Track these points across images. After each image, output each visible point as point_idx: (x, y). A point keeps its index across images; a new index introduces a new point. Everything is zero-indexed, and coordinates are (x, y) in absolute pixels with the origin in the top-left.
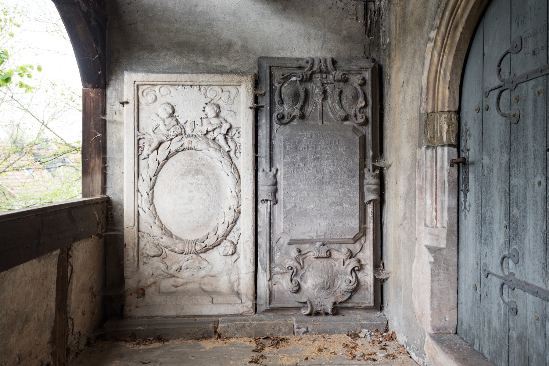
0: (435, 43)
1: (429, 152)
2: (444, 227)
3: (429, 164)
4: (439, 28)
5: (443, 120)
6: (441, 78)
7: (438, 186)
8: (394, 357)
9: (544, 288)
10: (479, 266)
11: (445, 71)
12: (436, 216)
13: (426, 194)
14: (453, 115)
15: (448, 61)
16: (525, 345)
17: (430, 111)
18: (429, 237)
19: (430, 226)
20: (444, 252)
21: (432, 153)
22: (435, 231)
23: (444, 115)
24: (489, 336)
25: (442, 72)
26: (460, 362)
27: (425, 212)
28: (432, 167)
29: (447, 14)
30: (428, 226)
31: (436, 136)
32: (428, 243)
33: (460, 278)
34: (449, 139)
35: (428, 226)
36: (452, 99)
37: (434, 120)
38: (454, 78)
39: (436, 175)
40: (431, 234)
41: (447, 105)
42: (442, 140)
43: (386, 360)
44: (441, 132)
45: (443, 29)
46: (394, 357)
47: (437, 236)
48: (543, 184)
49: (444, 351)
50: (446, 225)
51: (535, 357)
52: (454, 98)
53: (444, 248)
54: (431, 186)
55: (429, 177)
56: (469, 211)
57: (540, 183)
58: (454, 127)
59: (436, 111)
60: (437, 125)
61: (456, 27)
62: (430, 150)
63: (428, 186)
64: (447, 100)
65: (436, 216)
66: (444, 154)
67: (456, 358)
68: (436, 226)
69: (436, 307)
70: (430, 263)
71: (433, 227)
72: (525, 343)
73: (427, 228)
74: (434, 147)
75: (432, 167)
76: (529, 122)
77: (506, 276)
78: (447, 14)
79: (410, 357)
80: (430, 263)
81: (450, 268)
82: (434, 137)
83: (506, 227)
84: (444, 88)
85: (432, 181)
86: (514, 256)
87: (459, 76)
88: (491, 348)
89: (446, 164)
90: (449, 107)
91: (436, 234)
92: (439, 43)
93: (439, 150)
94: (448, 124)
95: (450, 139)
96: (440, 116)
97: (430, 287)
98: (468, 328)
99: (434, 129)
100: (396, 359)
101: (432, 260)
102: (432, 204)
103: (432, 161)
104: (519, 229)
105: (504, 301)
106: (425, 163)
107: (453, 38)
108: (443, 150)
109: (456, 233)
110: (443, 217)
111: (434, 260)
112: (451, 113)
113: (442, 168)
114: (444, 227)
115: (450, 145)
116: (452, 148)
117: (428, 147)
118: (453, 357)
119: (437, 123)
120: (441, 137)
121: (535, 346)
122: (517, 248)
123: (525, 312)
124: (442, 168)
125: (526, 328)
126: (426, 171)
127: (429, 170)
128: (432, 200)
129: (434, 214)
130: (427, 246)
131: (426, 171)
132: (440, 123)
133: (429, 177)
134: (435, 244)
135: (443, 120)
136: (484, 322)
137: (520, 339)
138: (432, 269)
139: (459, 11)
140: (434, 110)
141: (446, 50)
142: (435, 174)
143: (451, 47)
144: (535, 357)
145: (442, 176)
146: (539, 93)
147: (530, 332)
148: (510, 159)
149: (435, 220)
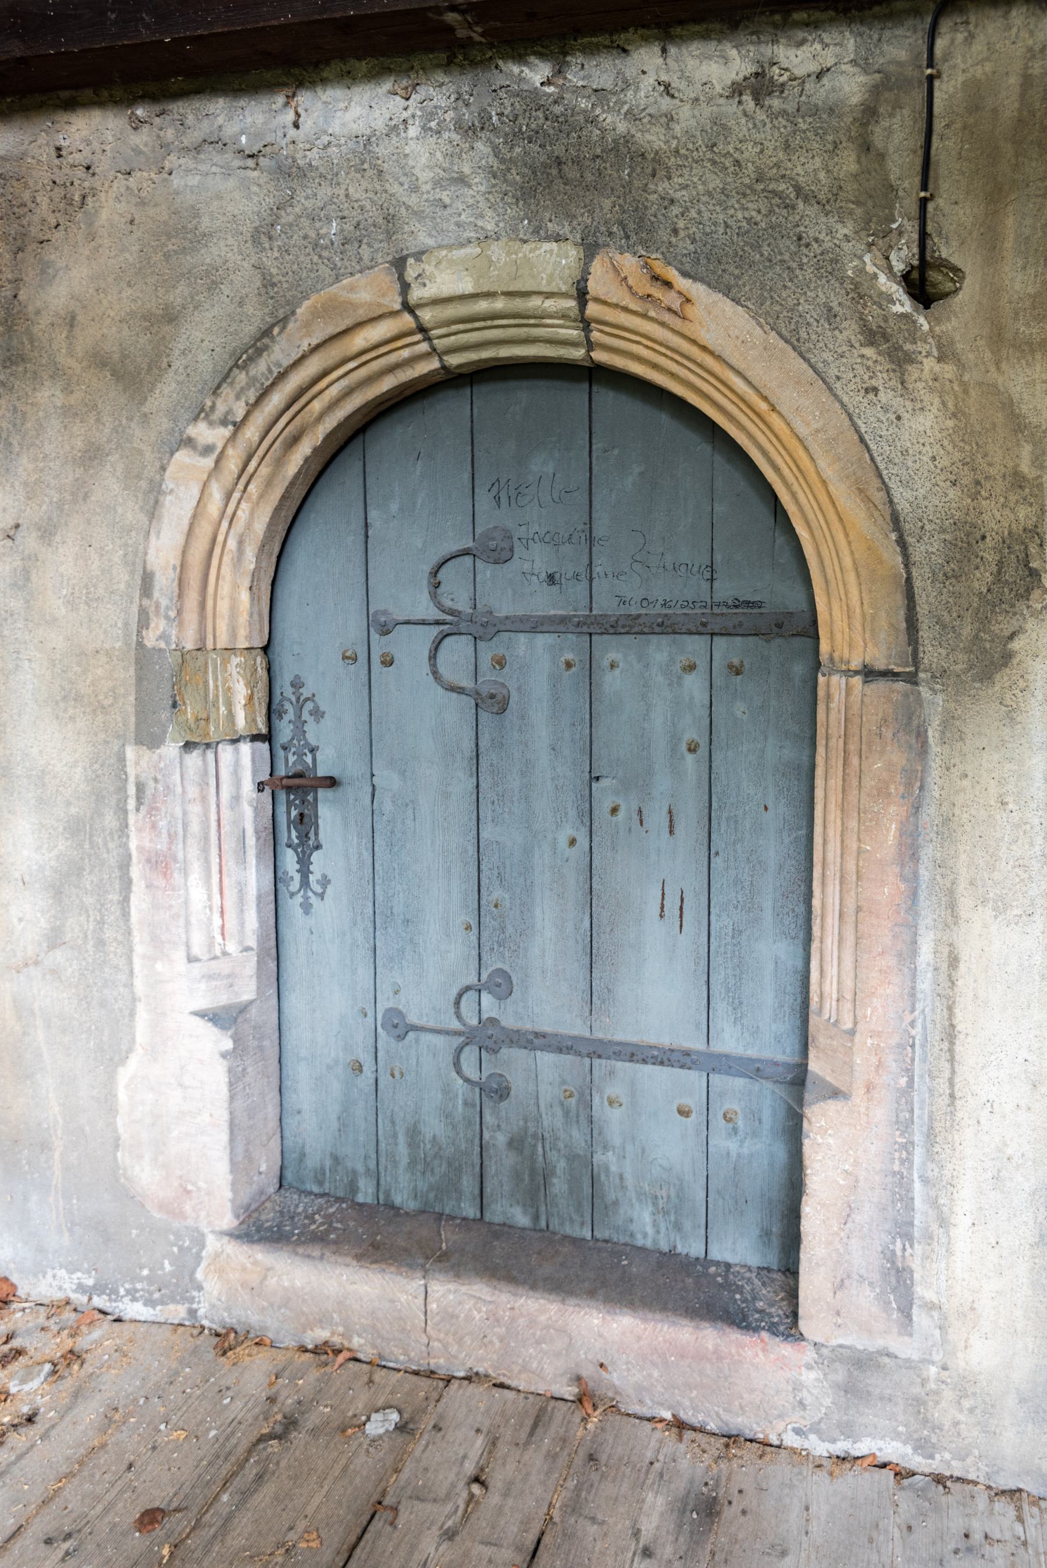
0: (218, 462)
1: (194, 759)
2: (247, 949)
3: (193, 792)
4: (238, 426)
5: (234, 673)
6: (226, 559)
7: (224, 847)
8: (74, 1356)
9: (587, 1034)
10: (370, 1019)
11: (241, 543)
12: (223, 926)
13: (186, 875)
14: (259, 659)
15: (256, 517)
16: (533, 1153)
17: (189, 646)
18: (203, 986)
19: (205, 957)
20: (253, 1011)
21: (204, 761)
22: (223, 966)
23: (236, 660)
24: (413, 1162)
25: (232, 544)
26: (376, 1262)
27: (188, 923)
28: (204, 799)
29: (276, 399)
30: (197, 960)
31: (213, 717)
32: (203, 1003)
33: (284, 1056)
34: (251, 720)
35: (197, 960)
36: (256, 617)
37: (206, 672)
38: (264, 564)
39: (219, 820)
40: (210, 977)
41: (242, 632)
42: (233, 724)
43: (68, 1384)
44: (229, 704)
45: (251, 432)
46: (74, 1356)
47: (229, 976)
48: (583, 841)
49: (309, 1256)
50: (252, 942)
51: (561, 1165)
52: (260, 615)
53: (251, 1002)
54: (205, 850)
55: (195, 827)
56: (322, 896)
57: (573, 842)
58: (261, 693)
59: (210, 645)
60: (216, 687)
61: (295, 440)
62: (196, 753)
63: (194, 851)
64: (243, 618)
65: (223, 926)
66: (242, 764)
67: (359, 1257)
68: (225, 954)
69: (240, 1158)
70: (224, 1055)
71: (215, 958)
72: (535, 1146)
73: (197, 965)
74: (208, 745)
75: (204, 799)
76: (539, 716)
77: (473, 1029)
78: (276, 399)
79: (118, 1320)
80: (224, 1055)
81: (266, 1043)
82: (207, 720)
83: (468, 928)
84: (235, 586)
85: (206, 838)
86: (499, 985)
87: (274, 560)
88: (420, 1184)
89: (248, 787)
90: (249, 637)
91: (226, 972)
92: (232, 465)
93: (226, 752)
94: (247, 684)
95: (254, 720)
96: (225, 662)
97: (226, 1116)
98: (328, 1163)
99: (206, 696)
100: (88, 1357)
101: (228, 1044)
102: (210, 898)
103: (203, 784)
104: (510, 930)
105: (467, 1080)
106: (179, 790)
107: (280, 463)
108: (237, 751)
109: (274, 951)
110: (242, 924)
111: (235, 1042)
112: (254, 652)
113: (236, 798)
114: (247, 949)
115: (255, 738)
116: (259, 745)
117: (188, 746)
118: (348, 1260)
119: (216, 680)
120: (231, 716)
121: (561, 1145)
122: (506, 968)
123: (531, 1087)
124: (236, 798)
125: (538, 1119)
126: (185, 813)
127: (195, 809)
128: (209, 889)
129: (217, 921)
130: (201, 1014)
131: (185, 813)
132: (225, 681)
133: (195, 827)
134: (224, 999)
135: (234, 673)
136: (395, 1136)
137: (516, 1143)
138: (230, 1071)
139: (317, 406)
140: (205, 645)
141: (252, 487)
142: (213, 817)
143: (269, 483)
144: (561, 1165)
145: (238, 821)
146: (569, 665)
147: (545, 1123)
148: (478, 787)
149: (219, 939)
